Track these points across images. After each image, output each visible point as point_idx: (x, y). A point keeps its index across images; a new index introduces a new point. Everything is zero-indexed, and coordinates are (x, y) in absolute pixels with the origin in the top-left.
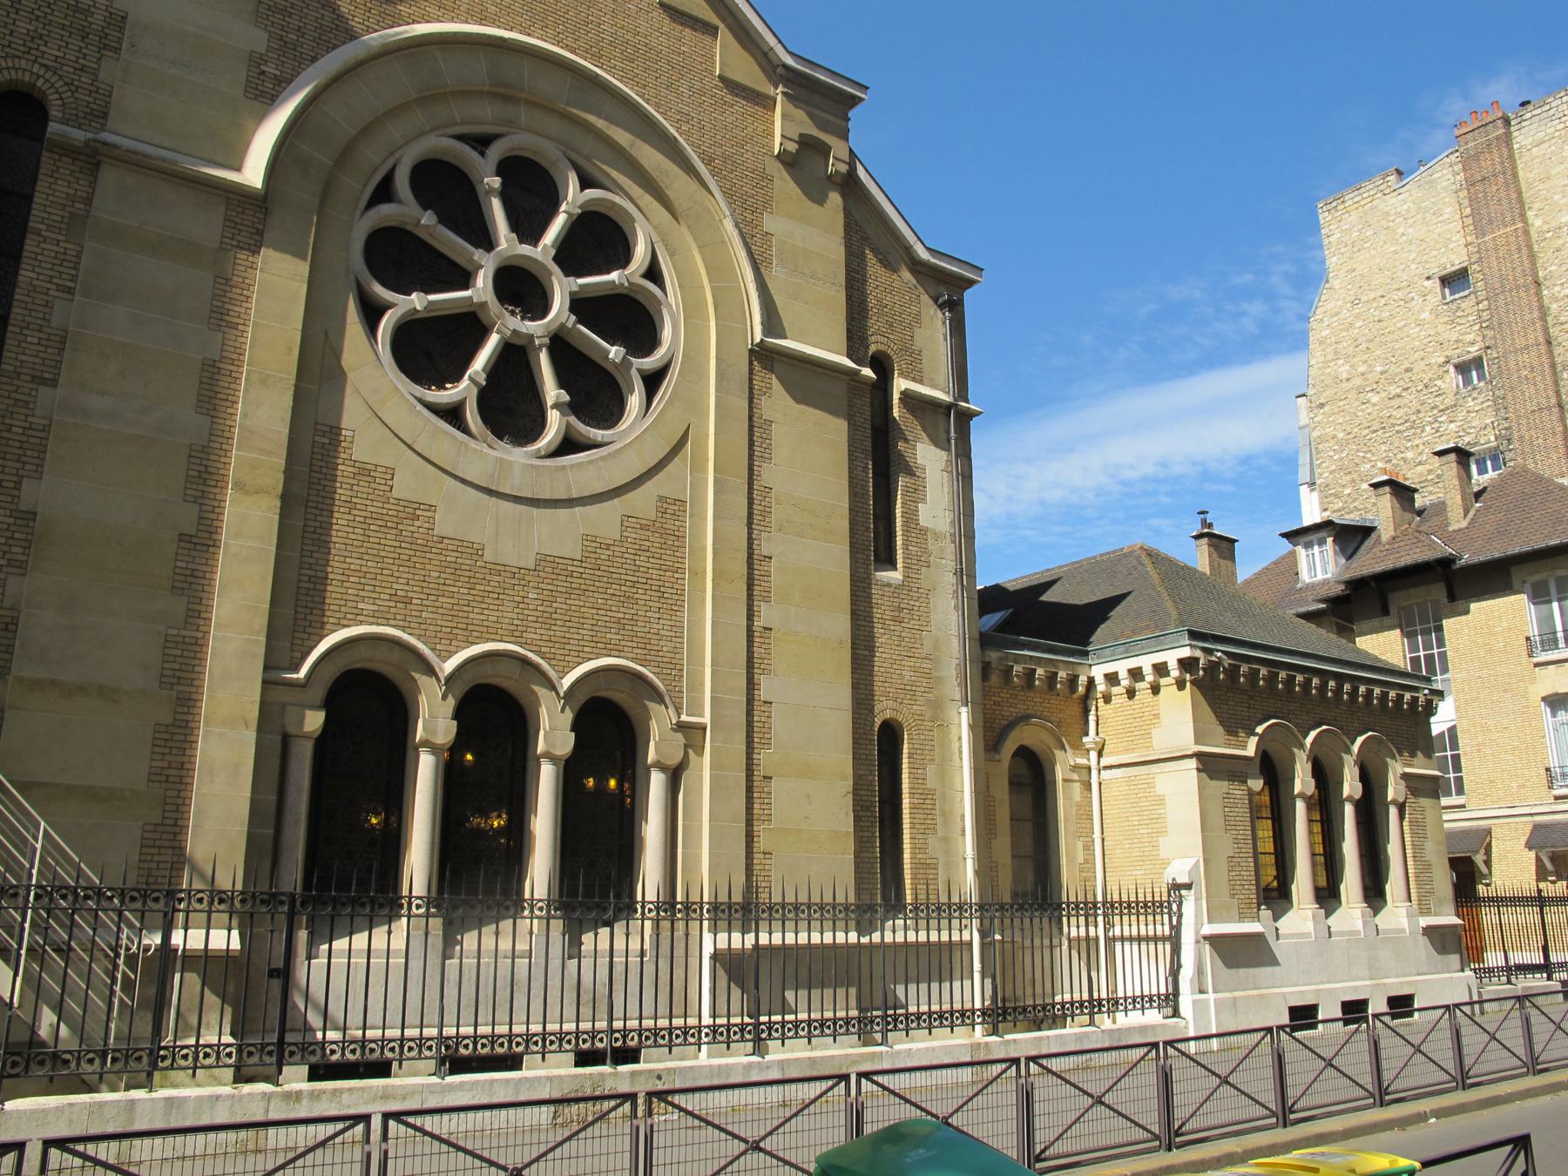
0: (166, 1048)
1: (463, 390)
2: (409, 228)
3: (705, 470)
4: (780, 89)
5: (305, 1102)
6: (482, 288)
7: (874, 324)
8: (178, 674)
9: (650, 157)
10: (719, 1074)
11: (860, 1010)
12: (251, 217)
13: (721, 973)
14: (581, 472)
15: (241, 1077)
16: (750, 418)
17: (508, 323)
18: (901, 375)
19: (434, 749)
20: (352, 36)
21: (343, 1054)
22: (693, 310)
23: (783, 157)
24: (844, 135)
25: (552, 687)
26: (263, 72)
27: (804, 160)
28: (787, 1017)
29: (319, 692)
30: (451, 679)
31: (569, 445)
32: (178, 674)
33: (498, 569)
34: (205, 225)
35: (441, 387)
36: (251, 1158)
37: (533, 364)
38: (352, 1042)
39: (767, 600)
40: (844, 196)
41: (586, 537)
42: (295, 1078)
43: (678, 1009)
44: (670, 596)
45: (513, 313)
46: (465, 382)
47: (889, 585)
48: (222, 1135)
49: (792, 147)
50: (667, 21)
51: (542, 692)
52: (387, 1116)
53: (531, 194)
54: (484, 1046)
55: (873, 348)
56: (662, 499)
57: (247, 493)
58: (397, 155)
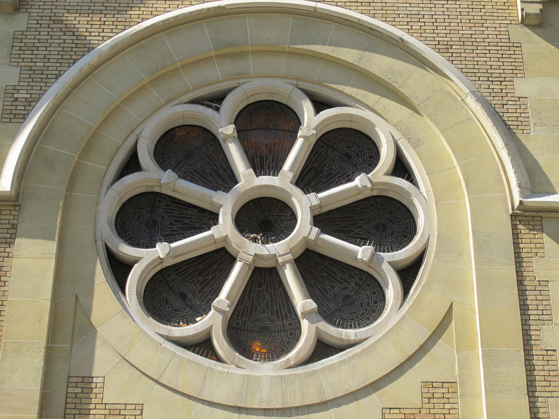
2: (157, 190)
9: (379, 64)
16: (520, 283)
17: (250, 250)
20: (90, 49)
22: (444, 194)
23: (527, 21)
31: (323, 349)
35: (190, 320)
45: (255, 240)
46: (305, 324)
56: (428, 385)
58: (137, 132)
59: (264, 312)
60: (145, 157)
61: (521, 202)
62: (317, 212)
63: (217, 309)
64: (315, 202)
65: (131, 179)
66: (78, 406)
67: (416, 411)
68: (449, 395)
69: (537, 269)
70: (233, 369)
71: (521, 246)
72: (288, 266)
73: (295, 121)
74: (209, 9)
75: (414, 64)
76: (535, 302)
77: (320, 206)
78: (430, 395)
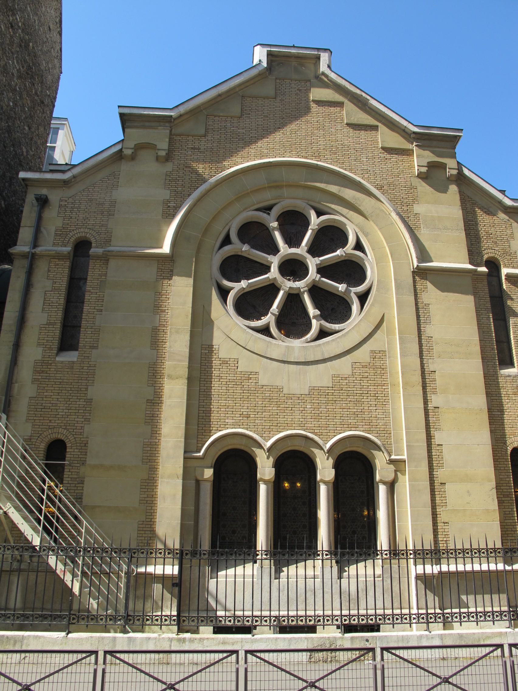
0: (149, 616)
1: (269, 319)
2: (240, 254)
3: (395, 335)
4: (415, 144)
5: (187, 643)
6: (274, 273)
7: (485, 244)
8: (149, 458)
9: (349, 194)
10: (403, 640)
11: (510, 607)
12: (167, 266)
13: (422, 586)
14: (330, 346)
15: (180, 630)
16: (416, 304)
17: (288, 285)
18: (505, 266)
19: (266, 482)
20: (205, 181)
21: (367, 621)
23: (420, 176)
24: (454, 156)
25: (321, 448)
26: (169, 207)
27: (433, 175)
28: (463, 610)
29: (211, 460)
30: (270, 449)
31: (323, 334)
32: (149, 458)
33: (290, 396)
34: (150, 272)
35: (259, 319)
36: (178, 667)
37: (302, 298)
38: (353, 616)
39: (435, 393)
40: (458, 186)
41: (333, 376)
42: (206, 632)
43: (396, 604)
44: (382, 399)
45: (289, 280)
46: (314, 322)
47: (509, 376)
48: (153, 655)
49: (424, 170)
50: (351, 130)
51: (316, 451)
52: (247, 652)
53: (293, 224)
54: (292, 621)
55: (485, 257)
56: (372, 352)
57: (173, 379)
58: (230, 224)
59: (294, 315)
60: (234, 237)
61: (417, 265)
62: (319, 267)
63: (272, 313)
64: (318, 262)
65: (227, 248)
66: (207, 359)
67: (368, 364)
68: (383, 357)
69: (424, 298)
70: (280, 343)
71: (417, 287)
72: (306, 293)
73: (306, 223)
74: (264, 163)
75: (365, 194)
76: (423, 314)
77: (320, 264)
78: (374, 357)
